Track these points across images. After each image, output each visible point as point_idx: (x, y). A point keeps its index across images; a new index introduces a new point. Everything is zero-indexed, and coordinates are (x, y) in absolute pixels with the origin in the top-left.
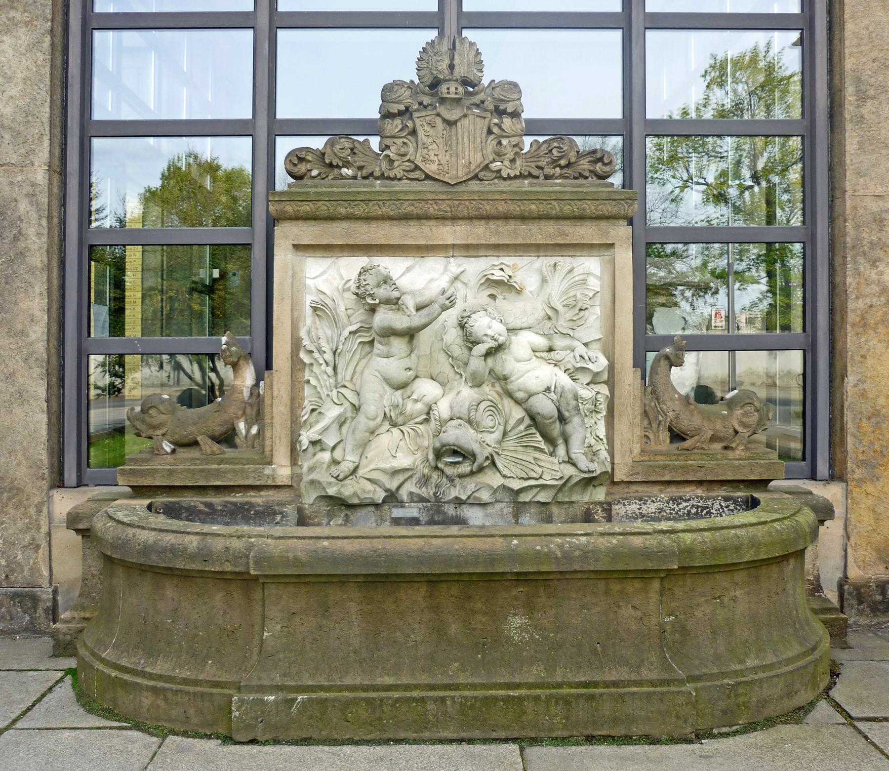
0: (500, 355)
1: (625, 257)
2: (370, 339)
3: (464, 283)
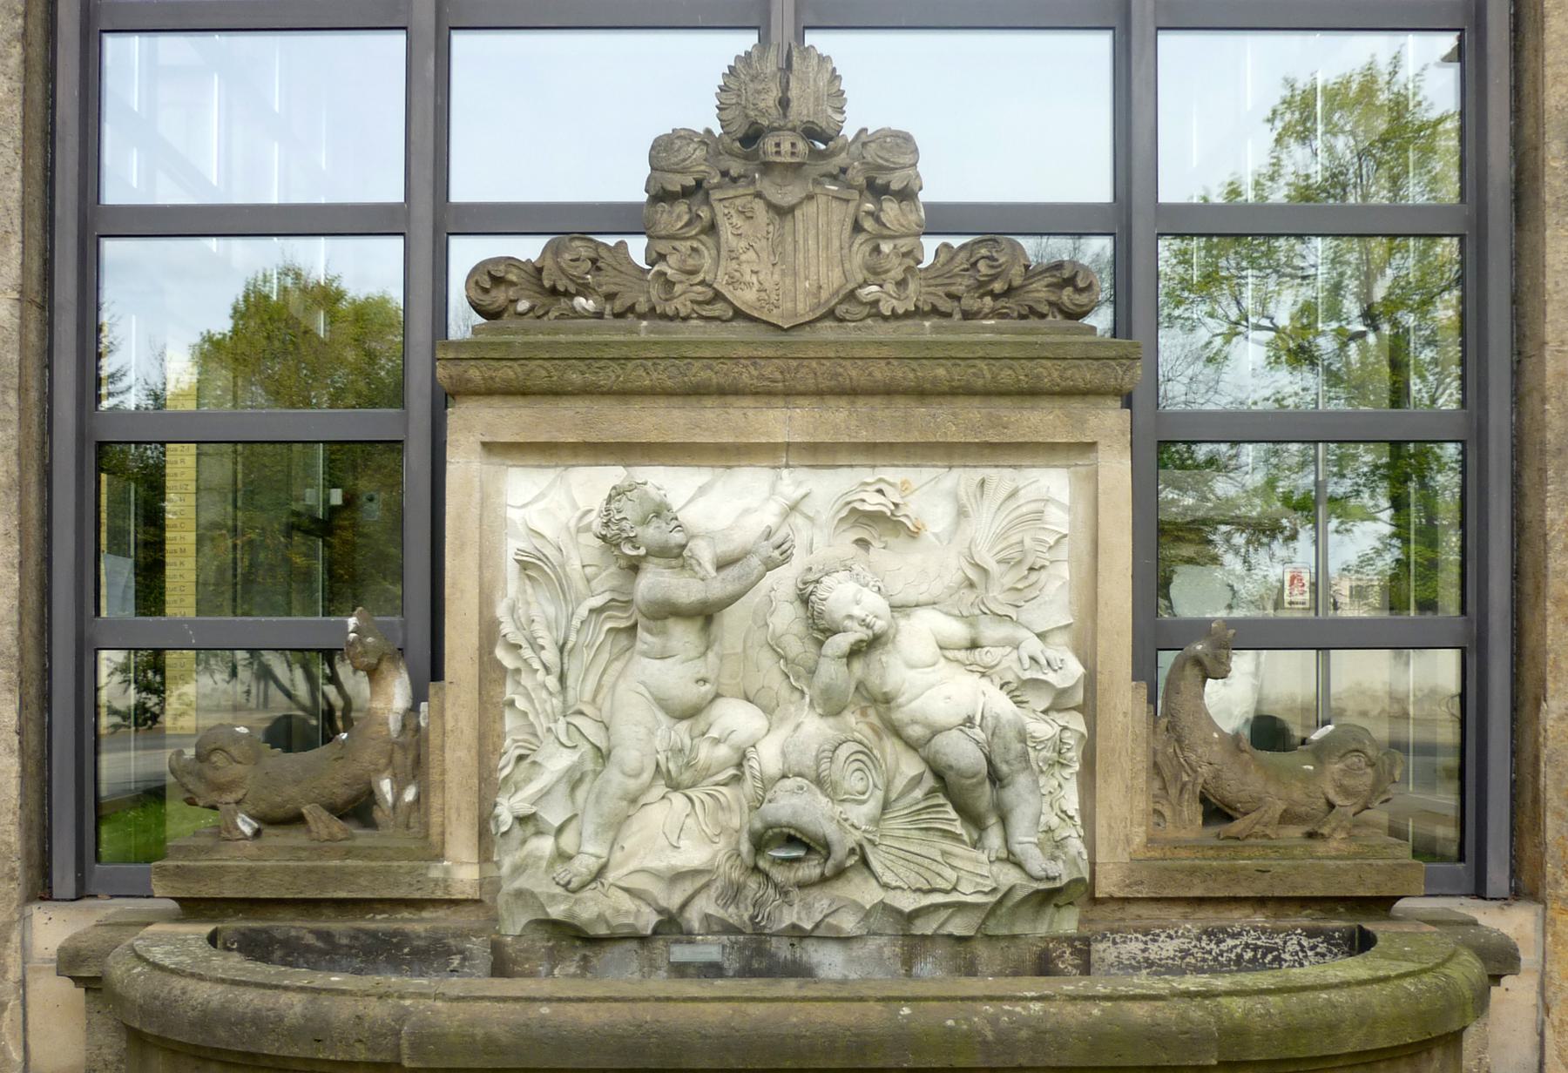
0: (878, 656)
1: (1116, 469)
3: (808, 517)
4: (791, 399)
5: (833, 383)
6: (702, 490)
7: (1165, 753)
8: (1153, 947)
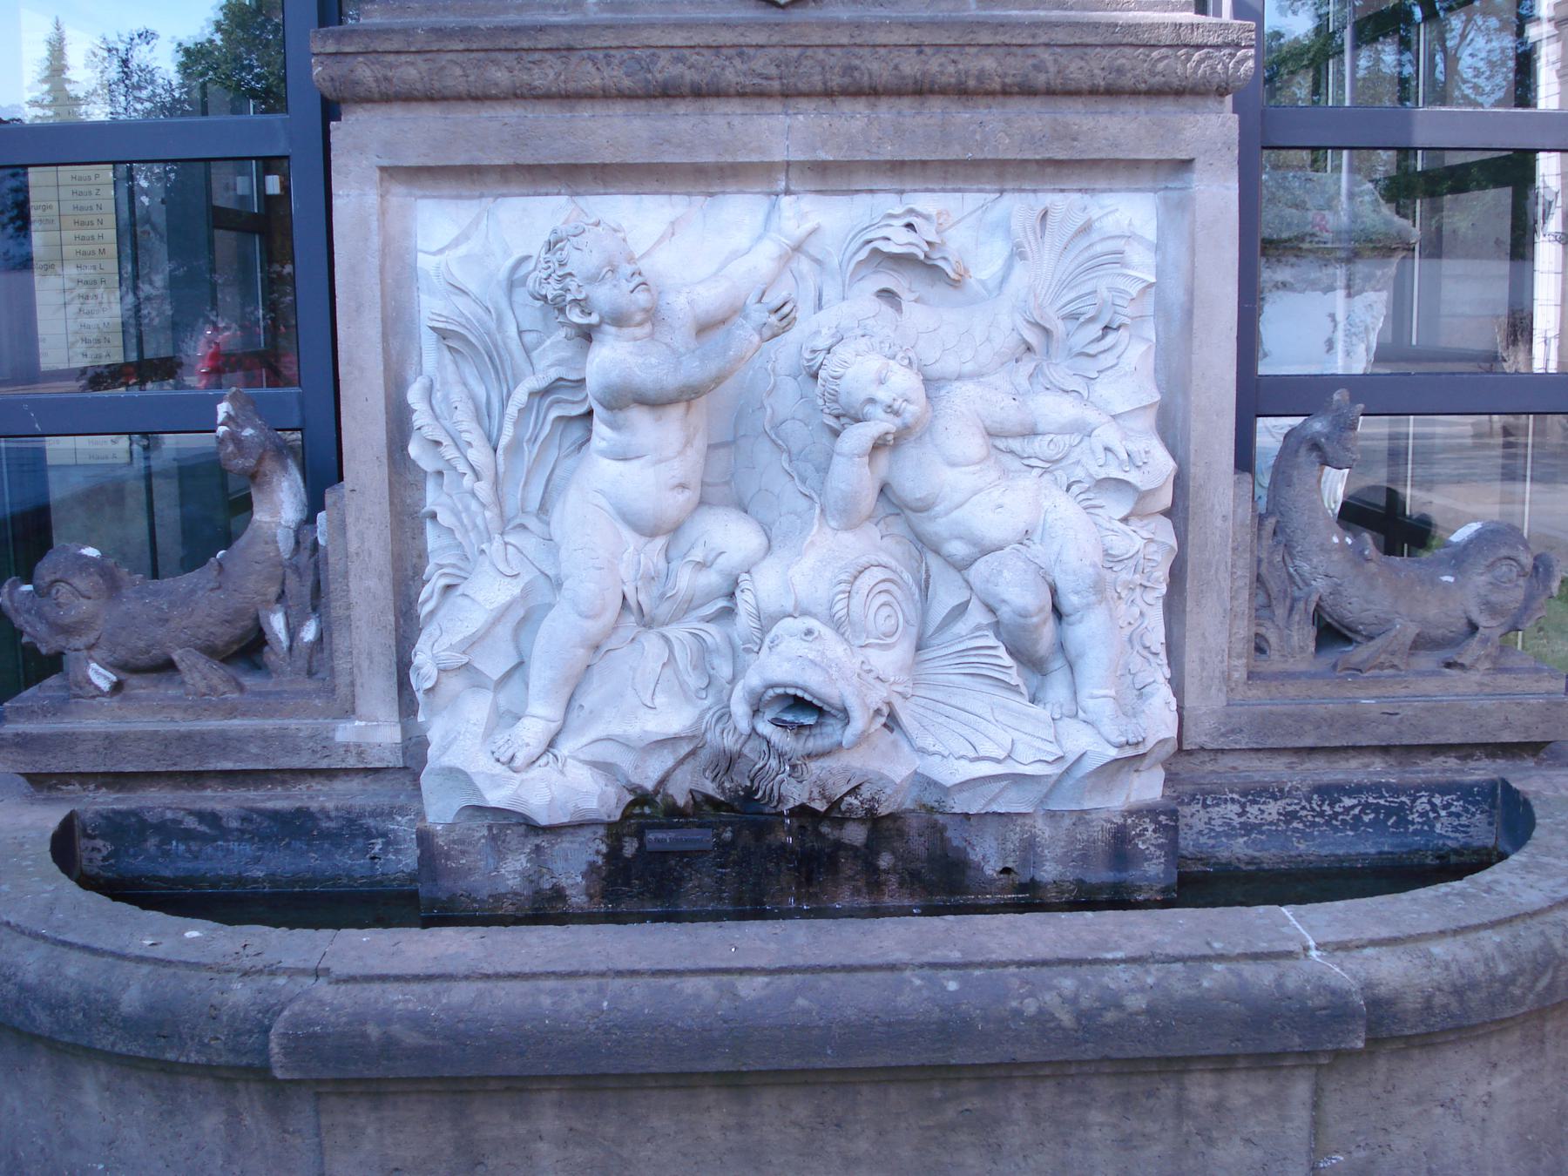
0: (910, 452)
1: (1217, 193)
2: (582, 409)
3: (817, 261)
4: (791, 102)
5: (847, 80)
6: (673, 228)
7: (1270, 563)
8: (1253, 810)
